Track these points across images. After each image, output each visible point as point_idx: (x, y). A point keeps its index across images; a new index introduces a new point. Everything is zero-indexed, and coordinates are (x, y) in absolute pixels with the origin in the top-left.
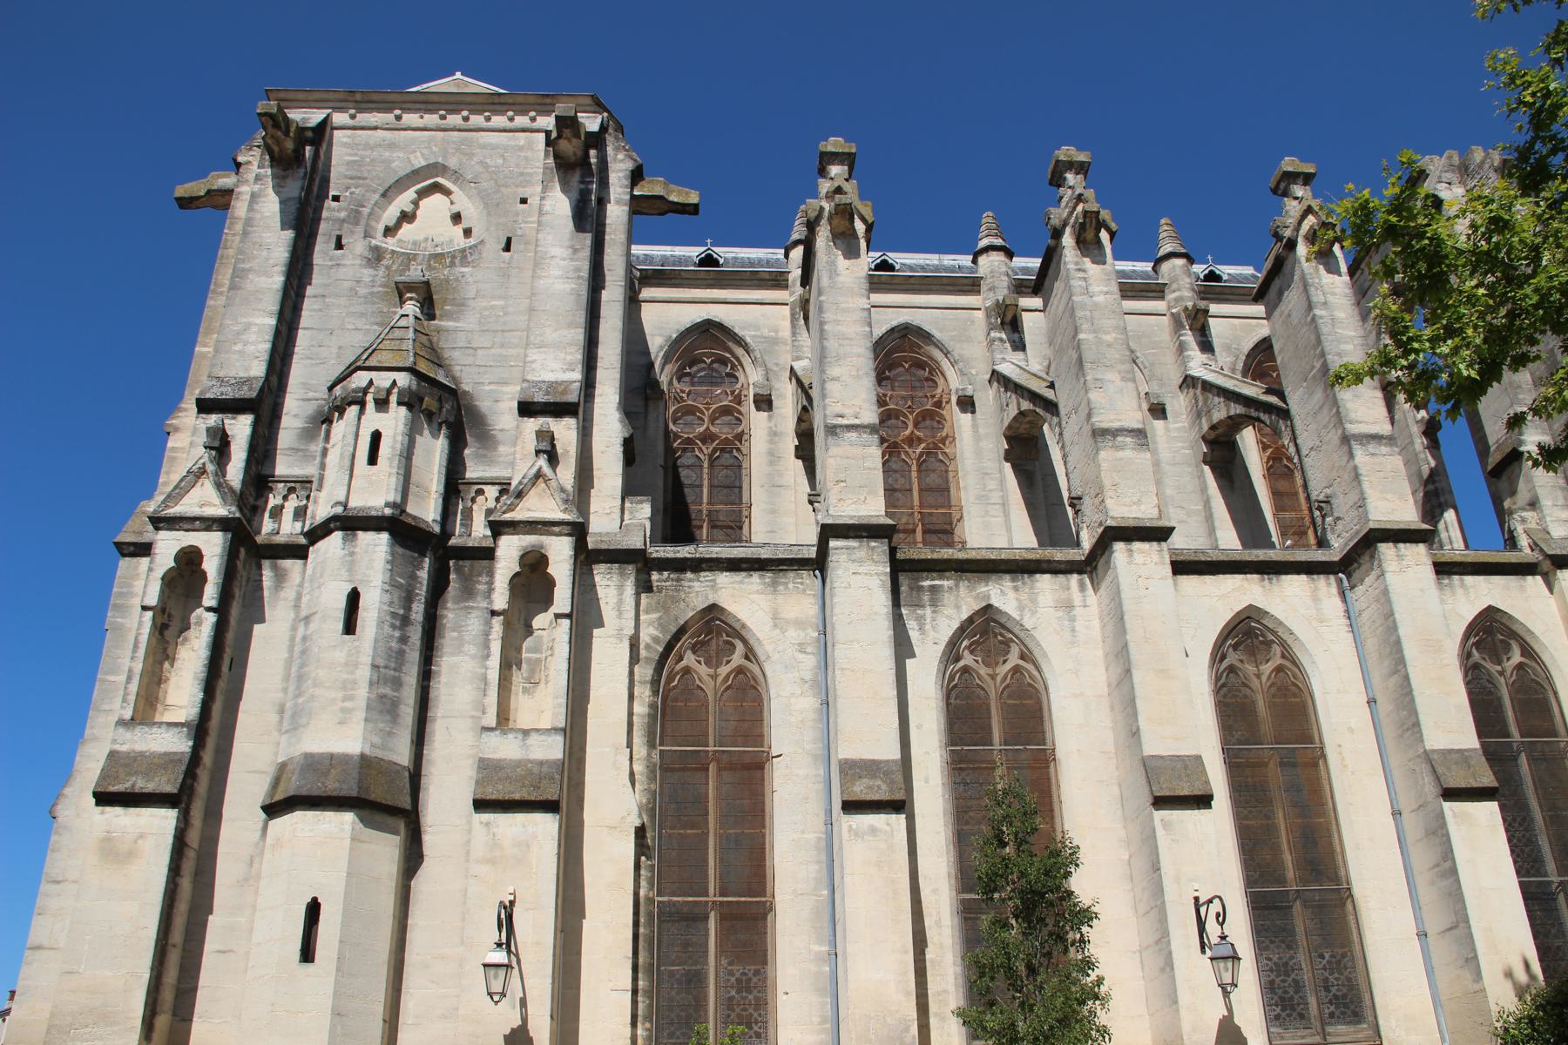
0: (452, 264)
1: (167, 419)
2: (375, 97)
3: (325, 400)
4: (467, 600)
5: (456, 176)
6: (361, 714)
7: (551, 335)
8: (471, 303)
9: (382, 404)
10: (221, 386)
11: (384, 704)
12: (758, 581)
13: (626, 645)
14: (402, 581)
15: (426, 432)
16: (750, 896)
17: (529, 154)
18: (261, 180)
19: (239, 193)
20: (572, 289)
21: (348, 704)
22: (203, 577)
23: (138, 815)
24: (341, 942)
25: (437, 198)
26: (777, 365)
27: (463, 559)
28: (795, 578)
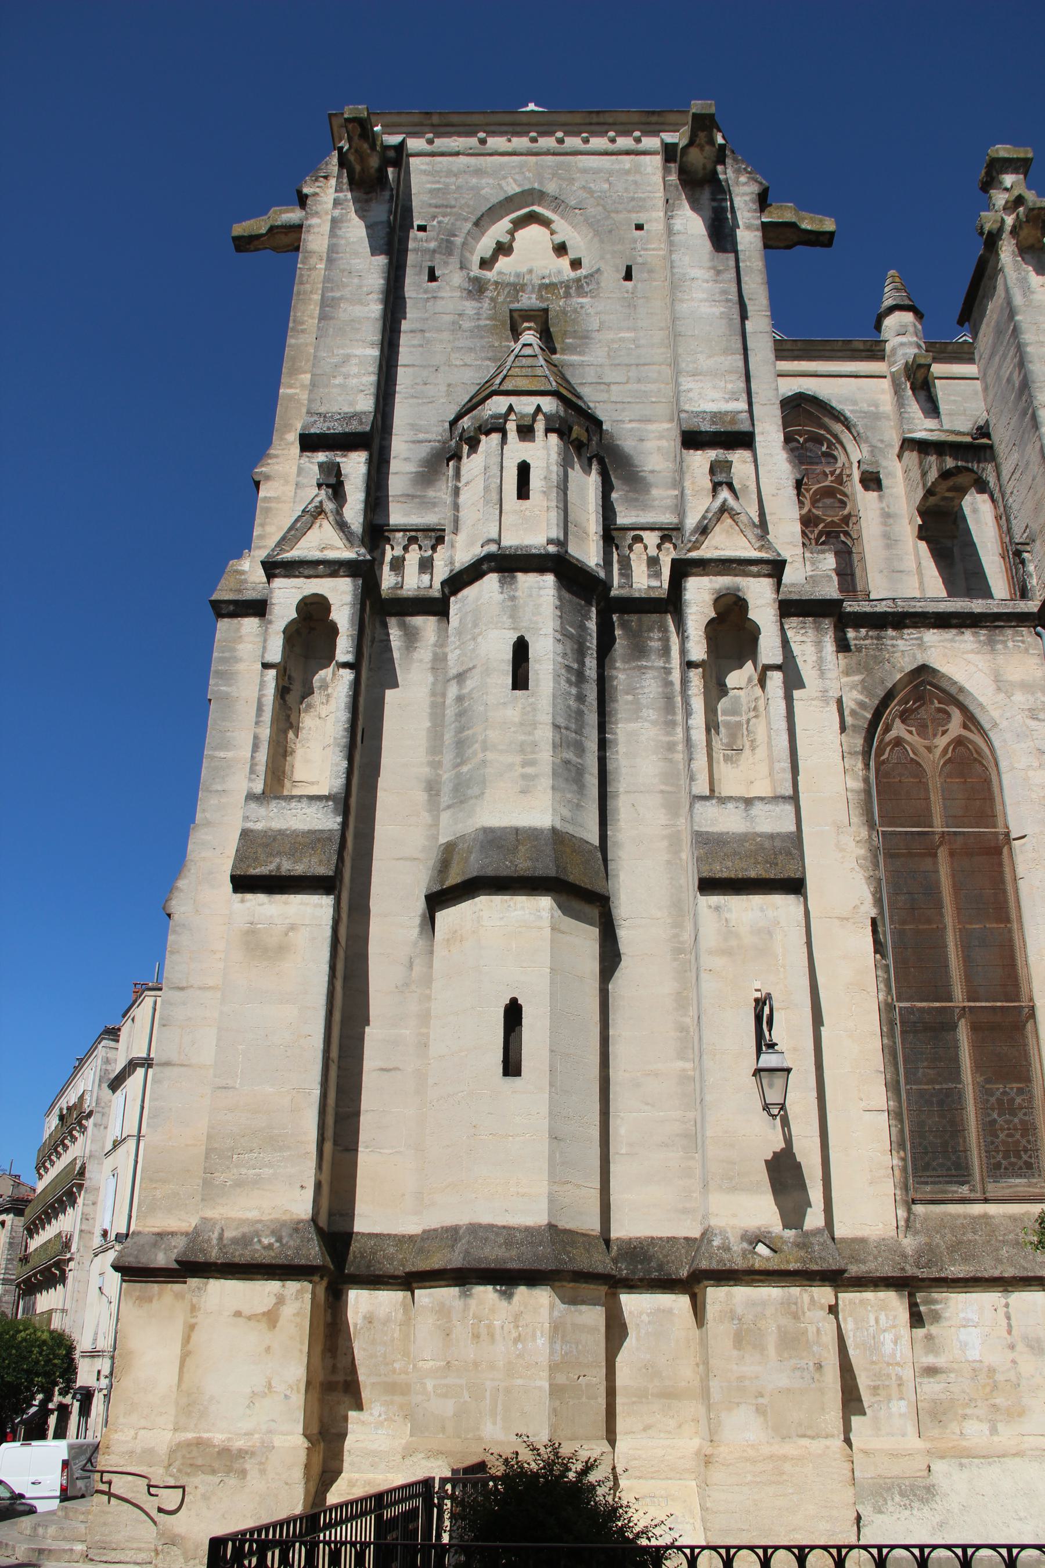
0: (567, 295)
1: (255, 467)
2: (455, 119)
3: (439, 441)
4: (639, 659)
5: (557, 203)
6: (546, 782)
7: (705, 362)
8: (595, 335)
9: (526, 432)
10: (325, 421)
11: (569, 770)
12: (972, 638)
13: (834, 708)
14: (573, 631)
15: (577, 466)
16: (1007, 1001)
17: (638, 178)
18: (340, 204)
19: (310, 226)
20: (722, 313)
21: (529, 770)
22: (333, 630)
23: (286, 903)
24: (552, 1051)
25: (534, 230)
26: (882, 441)
27: (629, 612)
28: (1013, 636)
